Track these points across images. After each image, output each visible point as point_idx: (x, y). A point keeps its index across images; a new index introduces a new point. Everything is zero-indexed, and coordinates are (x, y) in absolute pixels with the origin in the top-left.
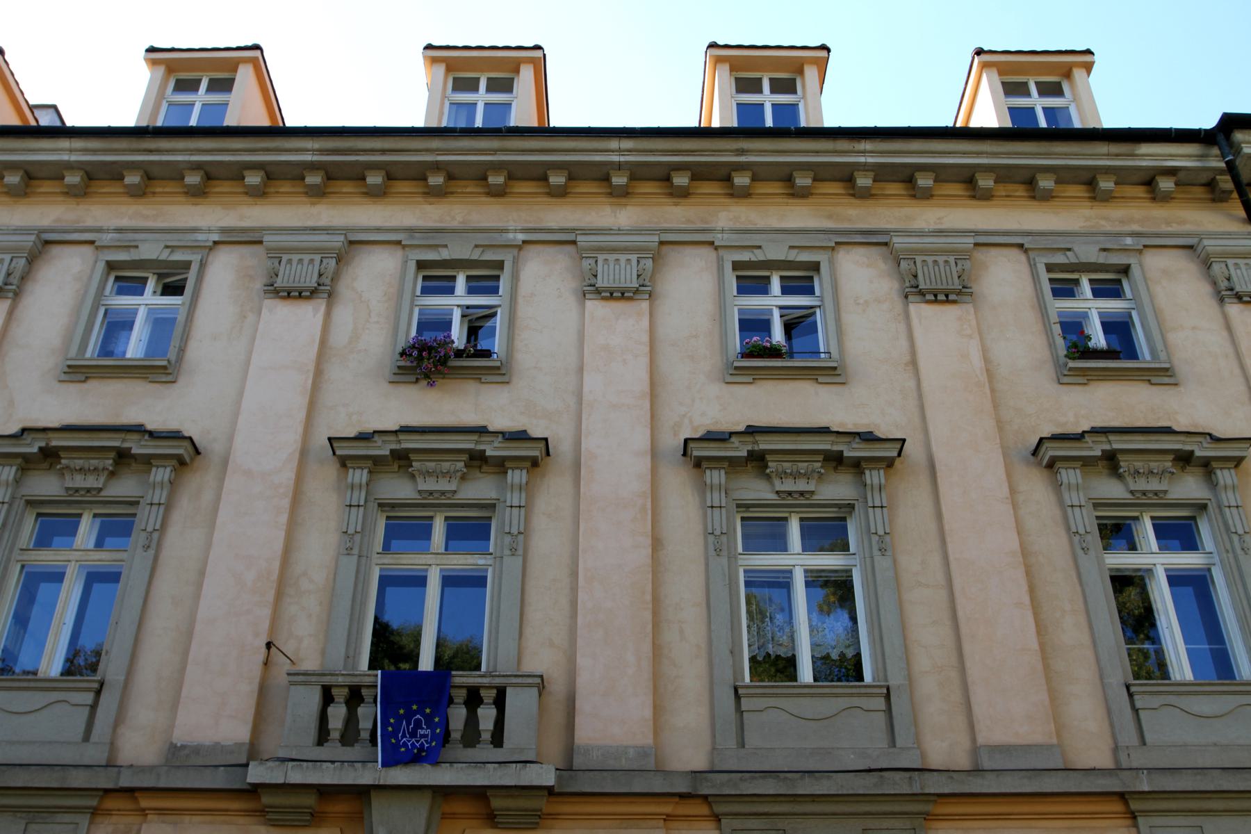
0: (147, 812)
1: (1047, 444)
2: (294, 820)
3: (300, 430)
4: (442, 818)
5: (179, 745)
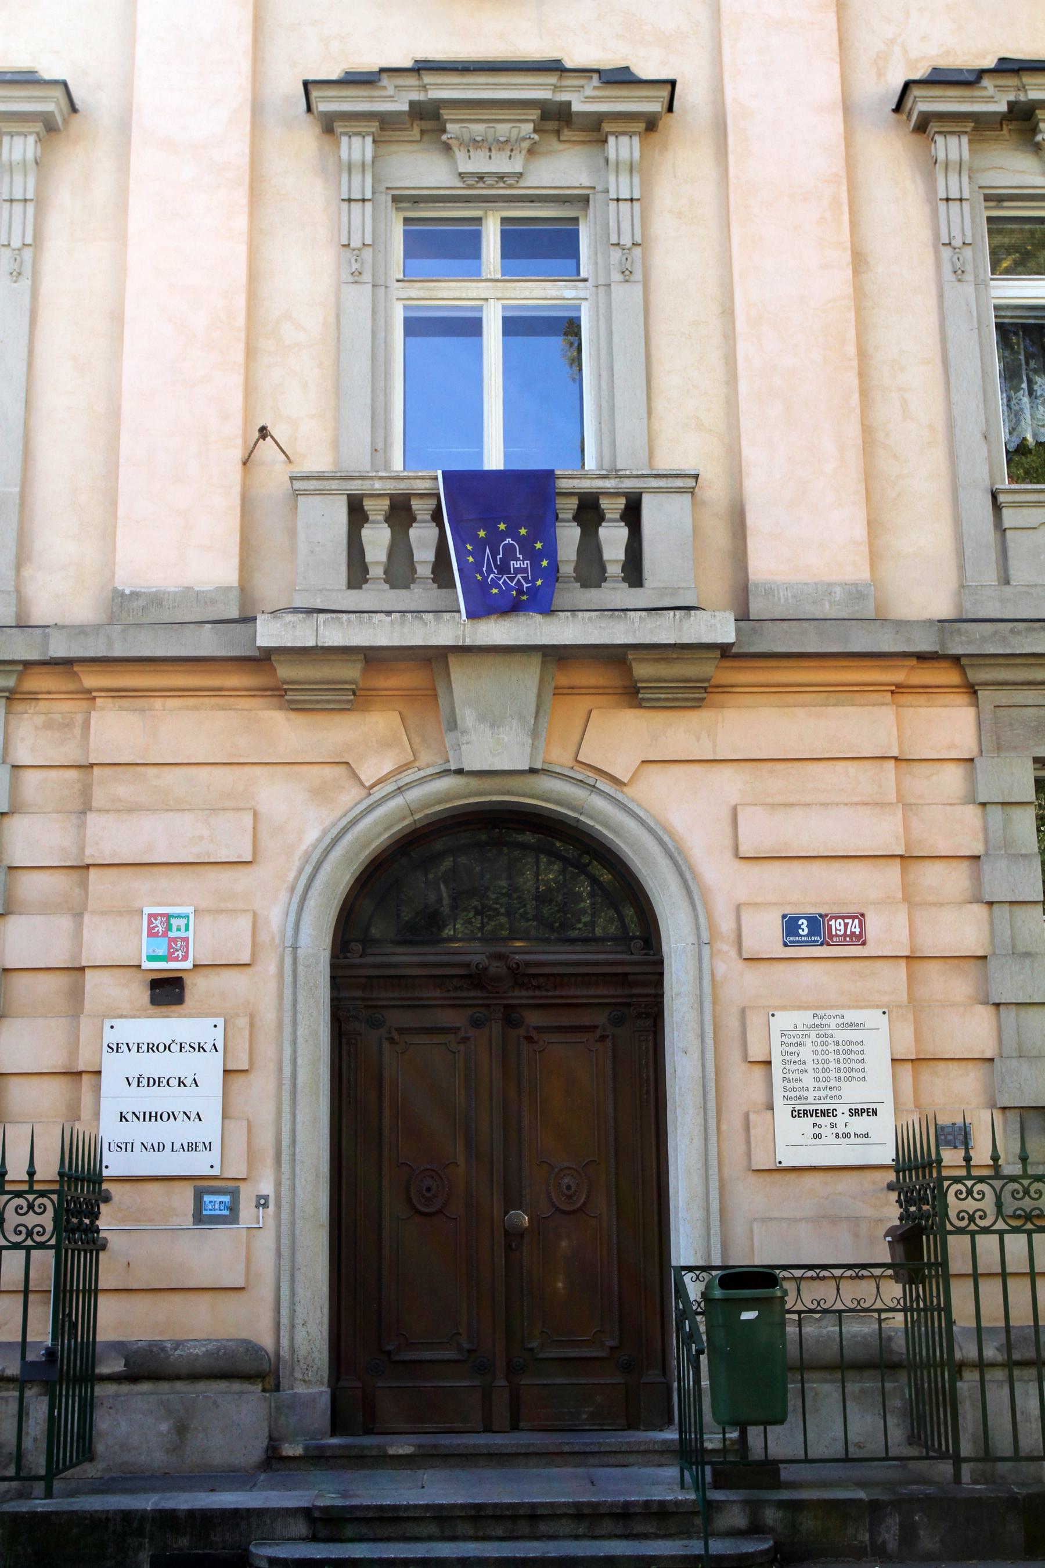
0: (94, 694)
1: (916, 92)
2: (328, 702)
3: (246, 66)
4: (554, 694)
5: (127, 592)
